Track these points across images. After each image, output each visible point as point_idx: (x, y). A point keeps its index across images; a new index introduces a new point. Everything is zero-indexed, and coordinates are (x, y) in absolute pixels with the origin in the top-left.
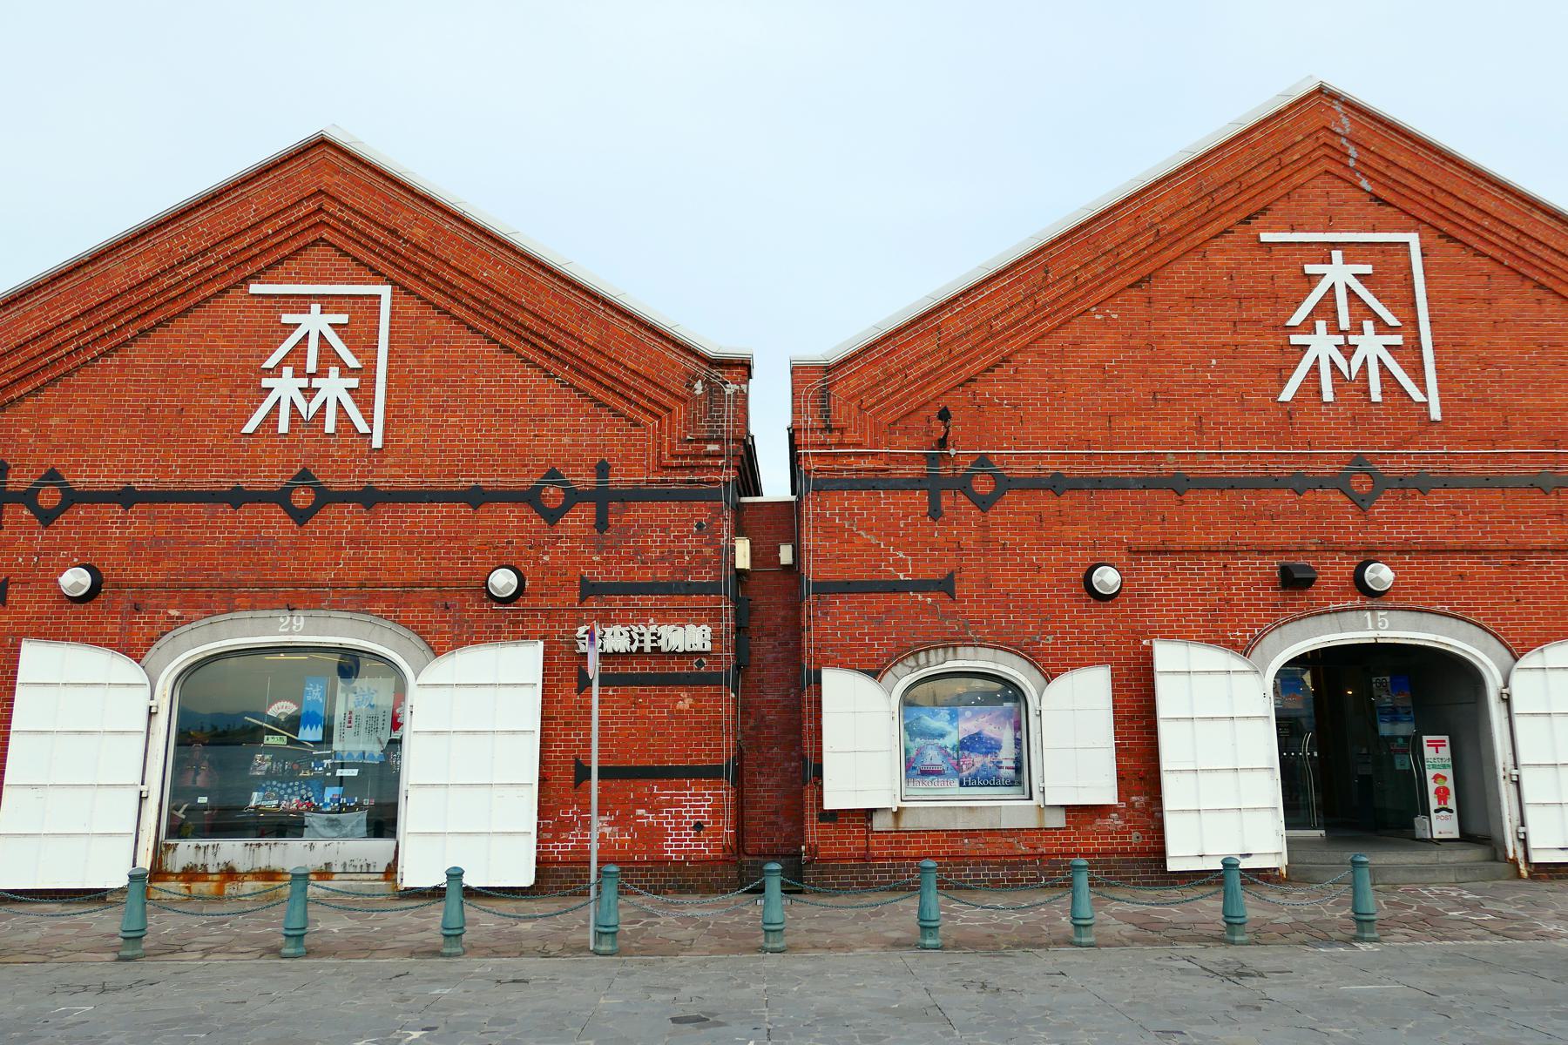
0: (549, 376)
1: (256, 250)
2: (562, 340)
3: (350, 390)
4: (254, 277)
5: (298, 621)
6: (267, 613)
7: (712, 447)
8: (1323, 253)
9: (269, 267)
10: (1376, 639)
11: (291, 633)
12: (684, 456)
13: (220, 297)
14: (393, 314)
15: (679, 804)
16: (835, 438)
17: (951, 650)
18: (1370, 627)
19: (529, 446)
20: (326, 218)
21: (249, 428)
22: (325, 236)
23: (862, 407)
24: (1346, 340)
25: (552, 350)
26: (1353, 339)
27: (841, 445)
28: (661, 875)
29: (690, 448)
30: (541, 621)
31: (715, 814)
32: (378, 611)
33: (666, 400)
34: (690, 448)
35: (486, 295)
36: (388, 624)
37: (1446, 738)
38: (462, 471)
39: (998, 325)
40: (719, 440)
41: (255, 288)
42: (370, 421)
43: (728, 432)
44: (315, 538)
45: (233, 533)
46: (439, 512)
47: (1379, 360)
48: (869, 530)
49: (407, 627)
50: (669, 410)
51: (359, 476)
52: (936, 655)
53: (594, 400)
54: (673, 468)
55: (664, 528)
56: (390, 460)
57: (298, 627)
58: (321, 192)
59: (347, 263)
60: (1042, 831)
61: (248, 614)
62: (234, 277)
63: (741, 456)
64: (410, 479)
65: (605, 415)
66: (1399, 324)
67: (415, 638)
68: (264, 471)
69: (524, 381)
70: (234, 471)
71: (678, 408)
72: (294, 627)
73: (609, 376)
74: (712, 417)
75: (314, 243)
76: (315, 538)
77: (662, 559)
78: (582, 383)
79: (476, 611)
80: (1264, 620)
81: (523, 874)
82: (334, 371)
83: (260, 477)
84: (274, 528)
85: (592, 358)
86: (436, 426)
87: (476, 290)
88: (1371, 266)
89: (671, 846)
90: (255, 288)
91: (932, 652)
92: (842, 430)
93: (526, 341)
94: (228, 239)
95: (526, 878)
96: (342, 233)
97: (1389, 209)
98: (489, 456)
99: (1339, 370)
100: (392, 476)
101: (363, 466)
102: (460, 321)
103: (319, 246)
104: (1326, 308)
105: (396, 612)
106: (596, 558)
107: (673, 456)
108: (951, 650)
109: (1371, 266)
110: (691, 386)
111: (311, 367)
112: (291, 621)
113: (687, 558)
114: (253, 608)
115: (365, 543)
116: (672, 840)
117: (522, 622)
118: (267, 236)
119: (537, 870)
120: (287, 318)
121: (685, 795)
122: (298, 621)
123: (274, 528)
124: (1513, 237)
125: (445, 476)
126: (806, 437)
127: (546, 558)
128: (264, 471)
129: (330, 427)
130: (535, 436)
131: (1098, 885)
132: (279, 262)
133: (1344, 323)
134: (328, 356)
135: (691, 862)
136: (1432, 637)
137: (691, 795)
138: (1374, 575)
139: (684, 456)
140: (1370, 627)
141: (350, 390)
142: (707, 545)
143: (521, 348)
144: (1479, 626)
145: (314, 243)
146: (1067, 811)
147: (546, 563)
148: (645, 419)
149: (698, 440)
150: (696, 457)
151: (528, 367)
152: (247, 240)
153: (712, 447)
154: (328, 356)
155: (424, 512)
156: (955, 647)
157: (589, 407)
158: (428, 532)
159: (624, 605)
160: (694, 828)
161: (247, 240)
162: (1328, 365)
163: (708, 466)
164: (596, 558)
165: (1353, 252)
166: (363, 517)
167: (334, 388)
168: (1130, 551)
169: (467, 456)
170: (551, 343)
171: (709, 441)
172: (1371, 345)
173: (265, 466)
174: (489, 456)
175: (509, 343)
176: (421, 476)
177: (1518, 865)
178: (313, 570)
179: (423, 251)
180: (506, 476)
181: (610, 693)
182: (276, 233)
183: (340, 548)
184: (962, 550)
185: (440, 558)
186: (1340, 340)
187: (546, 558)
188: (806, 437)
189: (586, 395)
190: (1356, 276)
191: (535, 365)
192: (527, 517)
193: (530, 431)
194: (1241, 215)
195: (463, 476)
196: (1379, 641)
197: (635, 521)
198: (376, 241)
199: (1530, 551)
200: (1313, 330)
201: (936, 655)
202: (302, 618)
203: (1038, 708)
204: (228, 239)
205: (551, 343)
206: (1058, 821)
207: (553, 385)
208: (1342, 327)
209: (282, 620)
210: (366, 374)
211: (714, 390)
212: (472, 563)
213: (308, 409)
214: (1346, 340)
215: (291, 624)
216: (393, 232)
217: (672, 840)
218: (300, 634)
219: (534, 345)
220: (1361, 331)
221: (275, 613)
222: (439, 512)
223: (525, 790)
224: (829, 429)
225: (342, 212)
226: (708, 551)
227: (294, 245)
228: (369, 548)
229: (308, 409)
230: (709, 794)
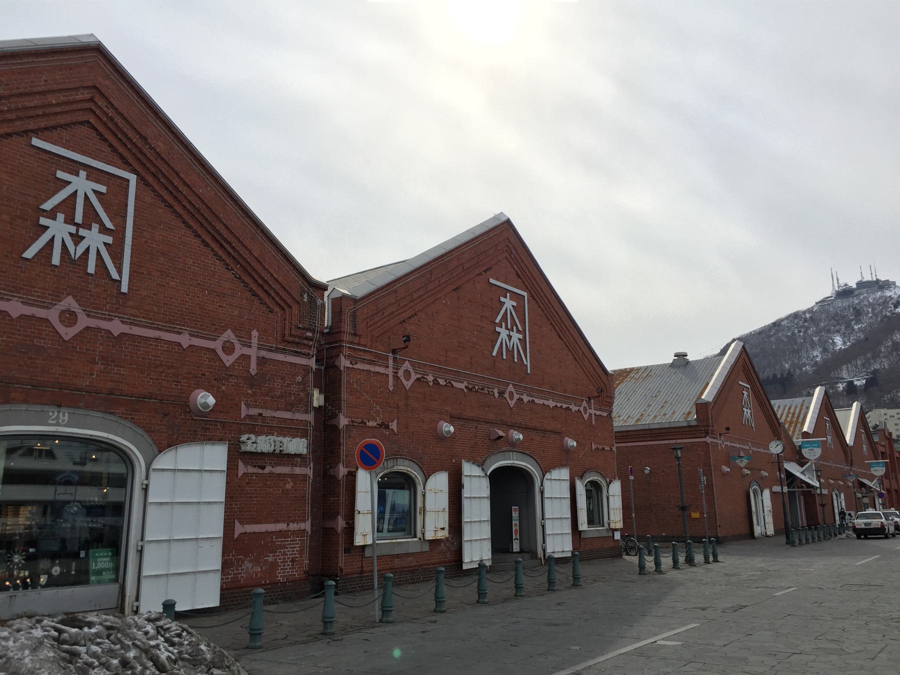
0: (228, 269)
1: (40, 112)
2: (240, 248)
3: (105, 244)
4: (37, 132)
5: (64, 416)
6: (38, 408)
7: (309, 334)
8: (74, 167)
9: (46, 129)
10: (512, 464)
11: (58, 424)
12: (295, 336)
13: (5, 138)
14: (137, 198)
15: (284, 547)
16: (356, 340)
17: (395, 460)
18: (512, 459)
19: (216, 312)
20: (94, 108)
21: (29, 254)
22: (92, 121)
23: (368, 326)
24: (77, 231)
25: (231, 251)
26: (82, 232)
27: (359, 344)
28: (277, 592)
29: (299, 332)
30: (219, 429)
31: (301, 552)
32: (119, 413)
33: (290, 301)
34: (299, 332)
35: (199, 205)
36: (128, 424)
37: (517, 507)
38: (177, 320)
39: (415, 296)
40: (313, 331)
41: (36, 142)
42: (120, 272)
43: (318, 327)
44: (77, 352)
45: (11, 338)
46: (161, 346)
47: (98, 251)
48: (367, 392)
49: (139, 426)
50: (290, 307)
51: (109, 311)
52: (390, 462)
53: (251, 290)
54: (288, 342)
55: (283, 378)
56: (130, 303)
57: (64, 420)
58: (95, 87)
59: (104, 147)
60: (422, 553)
61: (24, 407)
62: (18, 126)
63: (809, 450)
64: (144, 320)
65: (257, 302)
66: (113, 228)
67: (146, 435)
68: (38, 292)
69: (215, 268)
70: (13, 287)
71: (295, 308)
72: (60, 421)
73: (262, 278)
74: (311, 316)
75: (81, 123)
76: (77, 352)
77: (281, 397)
78: (247, 279)
79: (183, 419)
80: (486, 453)
81: (212, 600)
82: (95, 227)
83: (34, 296)
84: (45, 339)
85: (254, 264)
86: (161, 285)
87: (192, 198)
88: (105, 188)
89: (280, 573)
90: (36, 142)
91: (389, 461)
92: (360, 336)
93: (217, 241)
94: (21, 95)
95: (212, 600)
96: (105, 124)
97: (520, 280)
98: (194, 314)
99: (508, 346)
100: (133, 316)
101: (112, 304)
102: (179, 216)
103: (84, 125)
104: (68, 205)
105: (132, 415)
106: (249, 392)
107: (291, 335)
108: (395, 460)
109: (105, 188)
110: (302, 296)
111: (79, 218)
112: (58, 415)
113: (293, 397)
114: (25, 401)
115: (112, 361)
116: (281, 570)
117: (209, 429)
118: (51, 105)
119: (221, 595)
120: (60, 174)
121: (288, 541)
122: (64, 416)
123: (45, 339)
124: (547, 302)
125: (166, 322)
126: (346, 337)
127: (223, 388)
128: (38, 292)
129: (91, 269)
130: (220, 306)
131: (447, 578)
132: (55, 127)
133: (509, 327)
134: (91, 215)
135: (289, 582)
136: (105, 435)
137: (291, 541)
138: (203, 401)
139: (295, 336)
140: (512, 459)
141: (105, 244)
142: (302, 391)
143: (213, 245)
144: (536, 461)
145: (81, 123)
146: (430, 543)
147: (223, 392)
148: (277, 309)
149: (303, 329)
150: (300, 338)
151: (217, 259)
152: (36, 101)
153: (309, 334)
154: (91, 215)
155: (152, 345)
156: (397, 458)
157: (248, 294)
158: (155, 360)
159: (263, 423)
160: (291, 561)
161: (36, 101)
162: (95, 253)
163: (305, 345)
164: (249, 392)
165: (94, 174)
166: (111, 342)
167: (95, 239)
168: (451, 416)
169: (181, 311)
170: (233, 248)
171: (308, 330)
172: (516, 336)
173: (38, 288)
174: (194, 314)
175: (207, 240)
176: (151, 319)
177: (541, 560)
178: (74, 376)
179: (162, 159)
180: (203, 330)
181: (254, 478)
182: (58, 105)
183: (93, 362)
184: (399, 408)
185: (162, 379)
186: (73, 229)
187: (223, 388)
188: (346, 337)
189: (247, 287)
190: (95, 191)
191: (221, 259)
192: (213, 359)
193: (217, 302)
194: (485, 268)
195: (177, 324)
196: (513, 465)
197: (270, 371)
198: (130, 140)
199: (546, 431)
200: (54, 218)
201: (390, 462)
202: (67, 414)
203: (145, 482)
204: (21, 95)
205: (233, 248)
206: (426, 548)
207: (230, 275)
208: (76, 221)
209: (51, 414)
210: (118, 234)
211: (312, 300)
212: (181, 386)
213: (76, 251)
214: (77, 231)
215: (58, 418)
216: (144, 139)
217: (281, 570)
218: (65, 426)
219: (221, 246)
220: (89, 228)
221: (46, 408)
222: (161, 346)
223: (219, 540)
224: (355, 335)
225: (108, 109)
226: (302, 394)
227: (68, 119)
228: (114, 366)
229: (76, 251)
230: (299, 540)
